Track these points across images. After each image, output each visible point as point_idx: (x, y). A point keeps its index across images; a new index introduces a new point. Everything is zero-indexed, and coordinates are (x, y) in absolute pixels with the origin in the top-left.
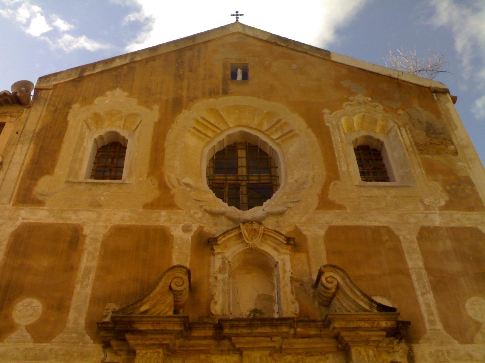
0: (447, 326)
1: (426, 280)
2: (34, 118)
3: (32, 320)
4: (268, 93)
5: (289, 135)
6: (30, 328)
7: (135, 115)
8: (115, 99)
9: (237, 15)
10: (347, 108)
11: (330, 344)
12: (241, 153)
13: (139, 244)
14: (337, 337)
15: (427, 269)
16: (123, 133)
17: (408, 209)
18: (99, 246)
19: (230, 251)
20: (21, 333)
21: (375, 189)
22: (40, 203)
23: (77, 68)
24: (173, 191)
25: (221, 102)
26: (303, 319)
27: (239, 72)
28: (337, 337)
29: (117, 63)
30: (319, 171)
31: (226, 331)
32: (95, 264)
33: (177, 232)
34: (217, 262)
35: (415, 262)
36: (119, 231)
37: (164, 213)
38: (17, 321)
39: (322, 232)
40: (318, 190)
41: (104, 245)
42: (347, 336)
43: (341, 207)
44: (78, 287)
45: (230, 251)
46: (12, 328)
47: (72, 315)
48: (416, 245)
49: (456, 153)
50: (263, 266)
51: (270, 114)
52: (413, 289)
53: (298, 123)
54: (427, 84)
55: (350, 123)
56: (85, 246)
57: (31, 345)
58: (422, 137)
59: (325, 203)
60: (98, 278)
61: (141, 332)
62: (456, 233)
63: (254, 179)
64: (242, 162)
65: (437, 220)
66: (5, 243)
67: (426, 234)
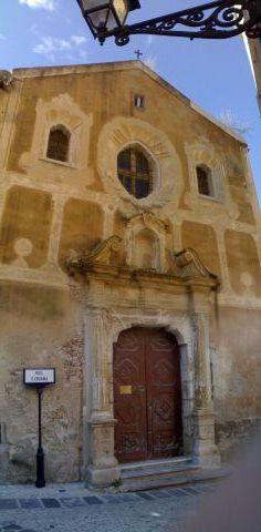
0: (233, 286)
1: (225, 260)
2: (13, 102)
3: (27, 253)
4: (155, 122)
5: (165, 155)
6: (27, 259)
7: (78, 118)
8: (64, 101)
9: (138, 53)
10: (197, 145)
11: (182, 290)
12: (133, 156)
13: (83, 213)
14: (189, 287)
15: (227, 254)
16: (69, 128)
17: (216, 215)
18: (62, 209)
19: (136, 227)
20: (20, 261)
21: (205, 201)
22: (23, 172)
23: (39, 68)
24: (103, 180)
25: (129, 121)
26: (168, 276)
27: (139, 100)
28: (189, 287)
29: (65, 72)
30: (180, 184)
31: (138, 277)
32: (61, 222)
33: (106, 209)
34: (128, 234)
35: (221, 249)
36: (73, 201)
37: (98, 194)
38: (18, 252)
39: (180, 224)
40: (179, 195)
41: (65, 210)
42: (194, 288)
43: (190, 210)
44: (52, 236)
45: (136, 227)
46: (15, 256)
47: (50, 253)
48: (223, 240)
49: (246, 187)
50: (148, 236)
51: (156, 138)
52: (219, 264)
53: (171, 148)
54: (238, 138)
55: (200, 151)
56: (55, 208)
57: (27, 269)
58: (231, 173)
59: (183, 206)
60: (63, 231)
61: (96, 273)
62: (242, 235)
63: (140, 176)
64: (133, 163)
65: (234, 226)
66: (4, 197)
67: (228, 233)
